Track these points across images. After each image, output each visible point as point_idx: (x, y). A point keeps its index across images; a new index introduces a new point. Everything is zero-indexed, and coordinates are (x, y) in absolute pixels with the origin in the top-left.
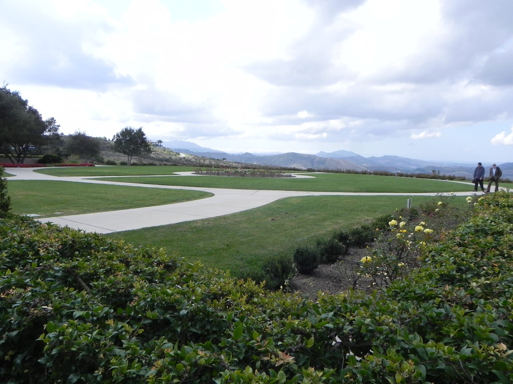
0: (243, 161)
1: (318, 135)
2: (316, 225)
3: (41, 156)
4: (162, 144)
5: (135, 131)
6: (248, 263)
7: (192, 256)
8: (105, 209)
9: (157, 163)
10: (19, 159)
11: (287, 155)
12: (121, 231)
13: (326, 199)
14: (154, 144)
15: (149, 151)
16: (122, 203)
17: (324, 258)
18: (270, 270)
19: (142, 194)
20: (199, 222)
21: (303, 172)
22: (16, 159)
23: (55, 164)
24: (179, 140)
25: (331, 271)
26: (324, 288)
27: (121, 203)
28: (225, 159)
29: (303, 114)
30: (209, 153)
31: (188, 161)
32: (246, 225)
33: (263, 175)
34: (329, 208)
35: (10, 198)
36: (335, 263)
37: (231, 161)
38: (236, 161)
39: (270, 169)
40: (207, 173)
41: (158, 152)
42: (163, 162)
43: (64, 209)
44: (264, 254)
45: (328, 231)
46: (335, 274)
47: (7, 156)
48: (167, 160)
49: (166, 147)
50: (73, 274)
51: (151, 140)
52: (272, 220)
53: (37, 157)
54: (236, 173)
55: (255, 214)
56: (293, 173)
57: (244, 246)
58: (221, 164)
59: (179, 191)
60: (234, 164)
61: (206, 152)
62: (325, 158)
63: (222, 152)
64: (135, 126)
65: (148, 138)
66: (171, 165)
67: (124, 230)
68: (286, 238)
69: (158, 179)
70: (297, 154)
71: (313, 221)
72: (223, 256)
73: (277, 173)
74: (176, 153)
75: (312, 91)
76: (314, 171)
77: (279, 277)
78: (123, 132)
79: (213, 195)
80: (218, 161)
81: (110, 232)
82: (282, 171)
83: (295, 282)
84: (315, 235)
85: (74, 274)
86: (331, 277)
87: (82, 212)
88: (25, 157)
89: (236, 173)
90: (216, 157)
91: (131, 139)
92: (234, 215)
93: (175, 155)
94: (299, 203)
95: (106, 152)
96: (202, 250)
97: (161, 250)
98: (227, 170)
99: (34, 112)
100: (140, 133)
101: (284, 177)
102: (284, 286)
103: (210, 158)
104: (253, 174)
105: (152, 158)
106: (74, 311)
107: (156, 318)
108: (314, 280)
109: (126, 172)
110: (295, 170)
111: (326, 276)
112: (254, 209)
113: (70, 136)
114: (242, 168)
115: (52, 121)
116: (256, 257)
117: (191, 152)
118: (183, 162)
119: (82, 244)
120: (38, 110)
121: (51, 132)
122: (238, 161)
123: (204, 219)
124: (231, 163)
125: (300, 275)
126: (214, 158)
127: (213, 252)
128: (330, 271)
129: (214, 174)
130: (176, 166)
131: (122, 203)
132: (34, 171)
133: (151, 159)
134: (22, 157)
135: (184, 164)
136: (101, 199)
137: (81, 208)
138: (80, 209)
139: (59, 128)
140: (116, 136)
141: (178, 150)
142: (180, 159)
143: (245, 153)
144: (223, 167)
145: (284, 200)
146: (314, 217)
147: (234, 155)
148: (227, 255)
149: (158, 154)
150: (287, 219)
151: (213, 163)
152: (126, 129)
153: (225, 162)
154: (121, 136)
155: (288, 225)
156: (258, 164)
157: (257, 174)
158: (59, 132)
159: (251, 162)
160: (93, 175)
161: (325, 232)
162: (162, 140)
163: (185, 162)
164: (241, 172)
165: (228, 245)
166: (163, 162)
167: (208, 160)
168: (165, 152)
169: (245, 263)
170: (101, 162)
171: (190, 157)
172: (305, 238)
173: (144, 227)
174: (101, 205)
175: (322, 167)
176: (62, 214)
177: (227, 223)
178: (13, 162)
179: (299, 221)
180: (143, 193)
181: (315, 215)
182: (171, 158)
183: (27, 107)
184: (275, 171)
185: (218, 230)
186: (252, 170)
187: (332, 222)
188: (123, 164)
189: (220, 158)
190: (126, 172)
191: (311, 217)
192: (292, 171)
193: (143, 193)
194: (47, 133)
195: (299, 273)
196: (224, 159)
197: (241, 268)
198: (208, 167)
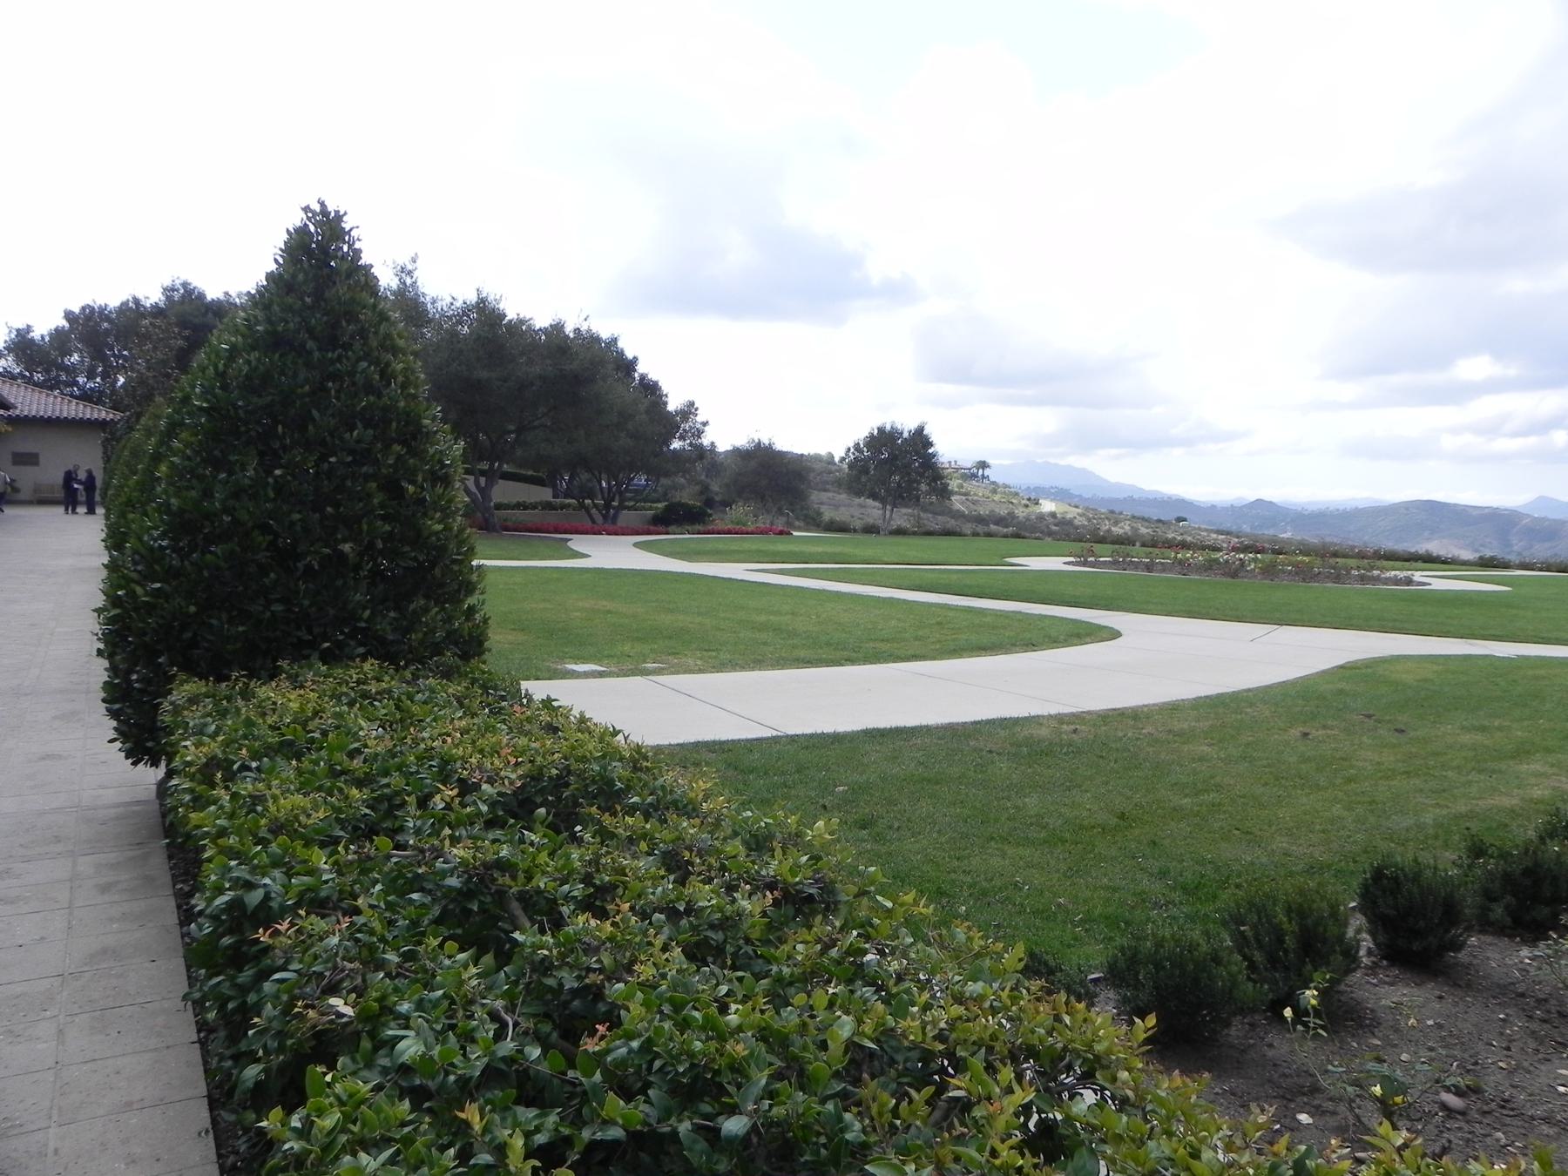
0: (1246, 528)
1: (1532, 441)
2: (1480, 771)
3: (659, 505)
4: (987, 472)
5: (906, 435)
6: (1185, 889)
7: (993, 843)
8: (778, 661)
9: (967, 528)
10: (608, 512)
11: (1407, 509)
12: (799, 732)
13: (1542, 672)
14: (965, 474)
15: (944, 493)
16: (831, 645)
17: (1498, 912)
18: (1250, 934)
19: (893, 623)
20: (1045, 722)
21: (1464, 567)
22: (600, 512)
23: (690, 528)
24: (1039, 461)
25: (1524, 971)
26: (1485, 1036)
27: (828, 644)
28: (1185, 520)
29: (1475, 368)
30: (1134, 500)
31: (1065, 523)
32: (1205, 748)
33: (1304, 574)
34: (1548, 706)
35: (489, 618)
36: (1542, 944)
37: (1203, 526)
38: (1221, 528)
39: (1335, 555)
40: (1115, 564)
41: (975, 495)
42: (988, 525)
43: (669, 654)
44: (1252, 864)
45: (1531, 800)
46: (1540, 983)
47: (582, 506)
48: (1000, 521)
49: (1000, 481)
50: (490, 889)
51: (956, 462)
52: (1306, 735)
53: (650, 509)
54: (1210, 566)
55: (1249, 710)
56: (1419, 573)
57: (1182, 825)
58: (1170, 536)
59: (1007, 617)
60: (1214, 536)
61: (1121, 496)
62: (1554, 520)
63: (1174, 498)
64: (906, 423)
65: (940, 453)
66: (1005, 536)
67: (809, 731)
68: (1350, 809)
69: (955, 577)
70: (1445, 503)
71: (1471, 754)
72: (1100, 853)
73: (1358, 568)
74: (1029, 499)
75: (1517, 285)
76: (1506, 565)
77: (1287, 969)
78: (872, 436)
79: (1114, 634)
80: (1161, 525)
81: (767, 733)
82: (1378, 563)
83: (1359, 994)
84: (1471, 811)
85: (494, 888)
86: (1522, 995)
87: (714, 667)
88: (622, 507)
89: (1210, 566)
90: (1154, 514)
91: (893, 458)
92: (1173, 708)
93: (1027, 506)
94: (1426, 680)
95: (830, 494)
96: (1031, 824)
97: (818, 828)
98: (1179, 556)
99: (651, 389)
100: (920, 440)
101: (1386, 584)
102: (1300, 1013)
103: (1134, 517)
104: (1269, 571)
105: (958, 515)
106: (403, 1037)
107: (639, 1127)
108: (1441, 997)
109: (869, 552)
110: (1429, 560)
111: (1499, 986)
112: (1249, 690)
113: (736, 452)
114: (1234, 549)
115: (689, 411)
116: (1217, 870)
117: (1077, 496)
118: (1048, 527)
119: (584, 779)
120: (660, 384)
121: (685, 440)
122: (1227, 526)
123: (1065, 715)
124: (1205, 534)
125: (1385, 968)
126: (1146, 516)
127: (1067, 835)
128: (1520, 970)
129: (1136, 566)
130: (1024, 538)
131: (831, 645)
132: (636, 545)
133: (952, 517)
134: (614, 508)
135: (1050, 534)
136: (774, 630)
137: (714, 654)
138: (710, 657)
139: (706, 428)
140: (852, 450)
141: (1037, 489)
142: (1041, 517)
143: (1252, 500)
144: (1171, 545)
145: (1367, 667)
146: (1479, 738)
147: (1213, 507)
148: (1114, 852)
149: (977, 501)
150: (1365, 739)
151: (1143, 531)
152: (881, 430)
153: (1181, 531)
154: (865, 449)
155: (1365, 760)
156: (1299, 538)
157: (1284, 572)
158: (706, 441)
159: (1271, 532)
160: (778, 559)
161: (1514, 802)
162: (988, 461)
163: (1054, 528)
164: (1227, 561)
165: (1122, 816)
166: (988, 525)
167: (1128, 522)
168: (997, 498)
169: (1174, 889)
170: (814, 522)
171: (1072, 513)
172: (1428, 818)
173: (870, 726)
174: (771, 649)
175: (1541, 551)
176: (663, 669)
177: (1140, 734)
178: (593, 521)
179: (1414, 750)
180: (899, 620)
181: (1483, 729)
182: (1012, 515)
183: (636, 375)
184: (1352, 562)
185: (1102, 757)
186: (1269, 557)
187: (1552, 765)
188: (871, 530)
189: (1169, 516)
190: (869, 552)
191: (1466, 738)
192: (1420, 565)
193: (899, 620)
194: (676, 444)
195: (1383, 958)
196: (1180, 519)
197: (1156, 905)
198: (1122, 543)
